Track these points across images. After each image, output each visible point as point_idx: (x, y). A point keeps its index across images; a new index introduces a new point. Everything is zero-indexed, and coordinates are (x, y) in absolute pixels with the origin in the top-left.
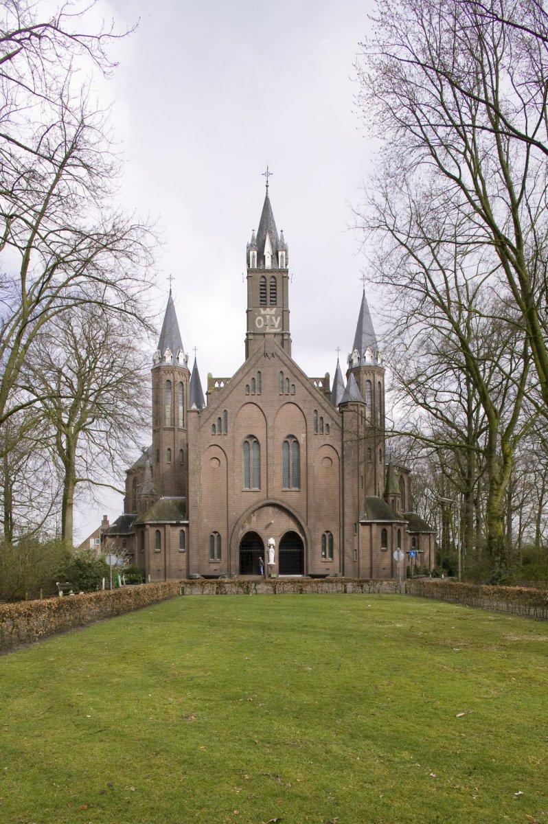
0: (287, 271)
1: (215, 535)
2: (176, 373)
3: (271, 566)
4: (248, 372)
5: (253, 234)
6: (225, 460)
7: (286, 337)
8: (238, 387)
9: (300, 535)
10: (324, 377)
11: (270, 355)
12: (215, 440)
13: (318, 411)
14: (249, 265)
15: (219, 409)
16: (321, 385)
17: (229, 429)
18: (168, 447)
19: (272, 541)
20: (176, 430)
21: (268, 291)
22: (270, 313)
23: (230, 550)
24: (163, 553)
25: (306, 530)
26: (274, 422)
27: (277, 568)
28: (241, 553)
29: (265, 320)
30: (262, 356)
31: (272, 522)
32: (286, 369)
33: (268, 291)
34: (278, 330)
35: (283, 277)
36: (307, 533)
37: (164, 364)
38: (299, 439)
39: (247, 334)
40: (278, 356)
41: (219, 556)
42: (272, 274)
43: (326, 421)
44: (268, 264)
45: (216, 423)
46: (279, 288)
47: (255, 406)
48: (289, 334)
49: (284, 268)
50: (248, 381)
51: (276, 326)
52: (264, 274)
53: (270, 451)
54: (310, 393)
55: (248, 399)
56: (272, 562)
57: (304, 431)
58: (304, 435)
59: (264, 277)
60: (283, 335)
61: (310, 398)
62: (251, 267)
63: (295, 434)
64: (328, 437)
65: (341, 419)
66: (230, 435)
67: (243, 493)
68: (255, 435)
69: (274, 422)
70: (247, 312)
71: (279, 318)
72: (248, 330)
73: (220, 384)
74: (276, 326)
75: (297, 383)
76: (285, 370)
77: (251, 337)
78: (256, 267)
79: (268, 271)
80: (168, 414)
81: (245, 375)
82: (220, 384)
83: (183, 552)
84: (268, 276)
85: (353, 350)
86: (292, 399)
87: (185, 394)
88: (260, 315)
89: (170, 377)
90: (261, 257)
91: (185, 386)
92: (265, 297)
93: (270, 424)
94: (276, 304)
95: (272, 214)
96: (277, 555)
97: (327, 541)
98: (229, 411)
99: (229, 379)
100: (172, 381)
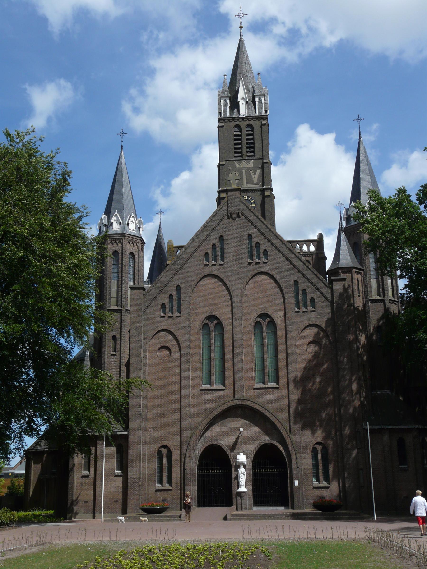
0: (266, 118)
1: (164, 451)
2: (125, 242)
3: (240, 494)
4: (207, 238)
5: (225, 79)
6: (178, 349)
7: (267, 193)
8: (194, 256)
9: (281, 448)
10: (316, 238)
11: (234, 216)
12: (165, 324)
13: (300, 281)
14: (220, 114)
15: (171, 284)
16: (312, 248)
17: (182, 308)
18: (113, 333)
19: (242, 458)
20: (124, 311)
21: (245, 141)
22: (246, 166)
23: (183, 471)
24: (92, 476)
25: (288, 441)
26: (241, 297)
27: (249, 499)
28: (199, 476)
29: (241, 173)
30: (224, 217)
31: (242, 429)
32: (255, 230)
33: (245, 141)
34: (258, 186)
35: (263, 125)
36: (290, 445)
37: (111, 232)
38: (275, 319)
39: (219, 192)
40: (245, 216)
41: (170, 482)
42: (248, 122)
43: (310, 295)
44: (243, 110)
45: (167, 302)
46: (257, 138)
47: (216, 281)
48: (272, 190)
49: (264, 113)
50: (207, 248)
51: (255, 181)
52: (238, 123)
53: (237, 334)
54: (288, 260)
55: (207, 271)
56: (243, 489)
57: (282, 307)
58: (282, 313)
59: (237, 126)
60: (263, 190)
61: (288, 265)
62: (223, 116)
63: (270, 313)
64: (313, 315)
65: (329, 291)
66: (184, 315)
67: (202, 392)
68: (218, 315)
69: (241, 297)
70: (219, 166)
71: (258, 172)
72: (219, 188)
73: (308, 247)
74: (255, 181)
75: (269, 248)
76: (254, 232)
77: (223, 195)
78: (228, 115)
79: (243, 118)
80: (114, 294)
81: (204, 241)
82: (308, 247)
83: (87, 477)
84: (243, 124)
85: (351, 203)
86: (265, 268)
87: (136, 267)
88: (234, 168)
89: (118, 248)
90: (235, 105)
91: (136, 257)
92: (240, 148)
93: (236, 300)
94: (254, 156)
95: (247, 56)
96: (251, 478)
97: (320, 456)
98: (182, 286)
99: (182, 247)
100: (120, 251)
